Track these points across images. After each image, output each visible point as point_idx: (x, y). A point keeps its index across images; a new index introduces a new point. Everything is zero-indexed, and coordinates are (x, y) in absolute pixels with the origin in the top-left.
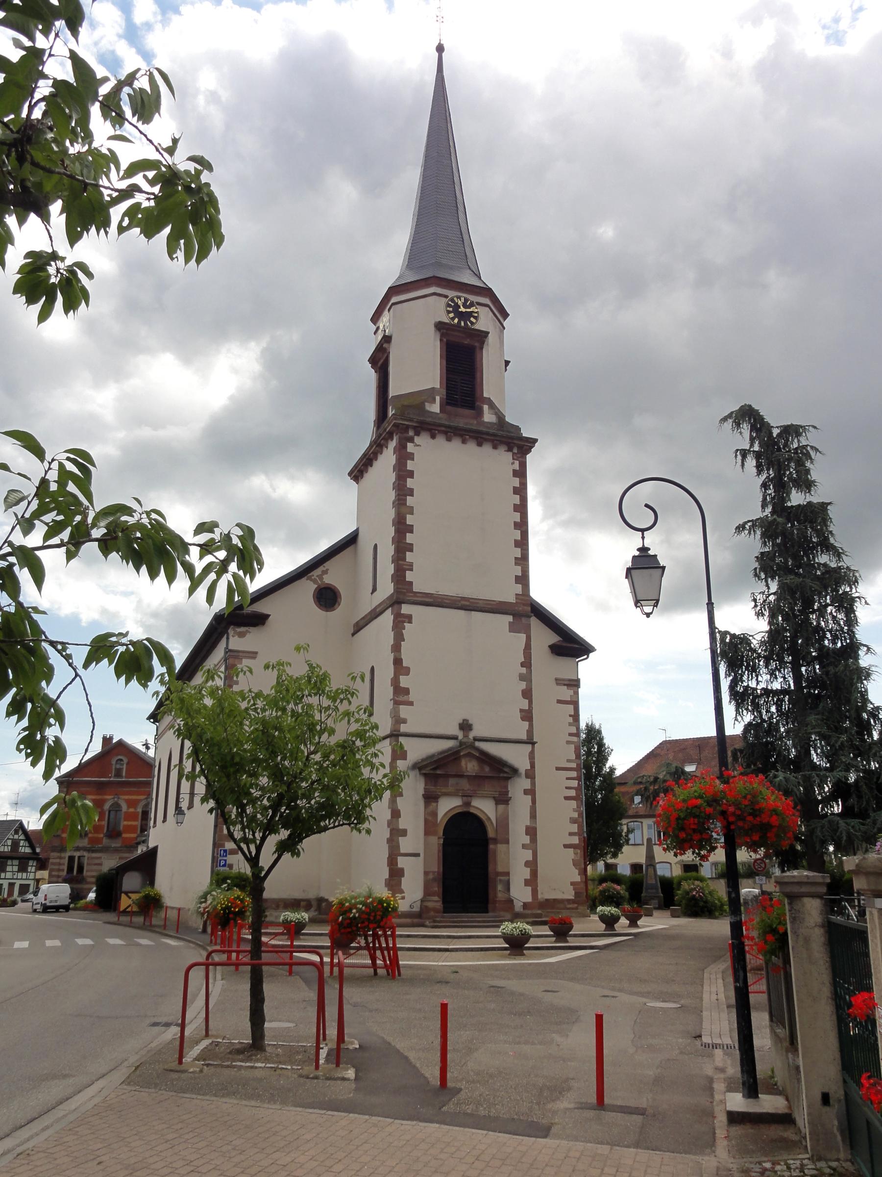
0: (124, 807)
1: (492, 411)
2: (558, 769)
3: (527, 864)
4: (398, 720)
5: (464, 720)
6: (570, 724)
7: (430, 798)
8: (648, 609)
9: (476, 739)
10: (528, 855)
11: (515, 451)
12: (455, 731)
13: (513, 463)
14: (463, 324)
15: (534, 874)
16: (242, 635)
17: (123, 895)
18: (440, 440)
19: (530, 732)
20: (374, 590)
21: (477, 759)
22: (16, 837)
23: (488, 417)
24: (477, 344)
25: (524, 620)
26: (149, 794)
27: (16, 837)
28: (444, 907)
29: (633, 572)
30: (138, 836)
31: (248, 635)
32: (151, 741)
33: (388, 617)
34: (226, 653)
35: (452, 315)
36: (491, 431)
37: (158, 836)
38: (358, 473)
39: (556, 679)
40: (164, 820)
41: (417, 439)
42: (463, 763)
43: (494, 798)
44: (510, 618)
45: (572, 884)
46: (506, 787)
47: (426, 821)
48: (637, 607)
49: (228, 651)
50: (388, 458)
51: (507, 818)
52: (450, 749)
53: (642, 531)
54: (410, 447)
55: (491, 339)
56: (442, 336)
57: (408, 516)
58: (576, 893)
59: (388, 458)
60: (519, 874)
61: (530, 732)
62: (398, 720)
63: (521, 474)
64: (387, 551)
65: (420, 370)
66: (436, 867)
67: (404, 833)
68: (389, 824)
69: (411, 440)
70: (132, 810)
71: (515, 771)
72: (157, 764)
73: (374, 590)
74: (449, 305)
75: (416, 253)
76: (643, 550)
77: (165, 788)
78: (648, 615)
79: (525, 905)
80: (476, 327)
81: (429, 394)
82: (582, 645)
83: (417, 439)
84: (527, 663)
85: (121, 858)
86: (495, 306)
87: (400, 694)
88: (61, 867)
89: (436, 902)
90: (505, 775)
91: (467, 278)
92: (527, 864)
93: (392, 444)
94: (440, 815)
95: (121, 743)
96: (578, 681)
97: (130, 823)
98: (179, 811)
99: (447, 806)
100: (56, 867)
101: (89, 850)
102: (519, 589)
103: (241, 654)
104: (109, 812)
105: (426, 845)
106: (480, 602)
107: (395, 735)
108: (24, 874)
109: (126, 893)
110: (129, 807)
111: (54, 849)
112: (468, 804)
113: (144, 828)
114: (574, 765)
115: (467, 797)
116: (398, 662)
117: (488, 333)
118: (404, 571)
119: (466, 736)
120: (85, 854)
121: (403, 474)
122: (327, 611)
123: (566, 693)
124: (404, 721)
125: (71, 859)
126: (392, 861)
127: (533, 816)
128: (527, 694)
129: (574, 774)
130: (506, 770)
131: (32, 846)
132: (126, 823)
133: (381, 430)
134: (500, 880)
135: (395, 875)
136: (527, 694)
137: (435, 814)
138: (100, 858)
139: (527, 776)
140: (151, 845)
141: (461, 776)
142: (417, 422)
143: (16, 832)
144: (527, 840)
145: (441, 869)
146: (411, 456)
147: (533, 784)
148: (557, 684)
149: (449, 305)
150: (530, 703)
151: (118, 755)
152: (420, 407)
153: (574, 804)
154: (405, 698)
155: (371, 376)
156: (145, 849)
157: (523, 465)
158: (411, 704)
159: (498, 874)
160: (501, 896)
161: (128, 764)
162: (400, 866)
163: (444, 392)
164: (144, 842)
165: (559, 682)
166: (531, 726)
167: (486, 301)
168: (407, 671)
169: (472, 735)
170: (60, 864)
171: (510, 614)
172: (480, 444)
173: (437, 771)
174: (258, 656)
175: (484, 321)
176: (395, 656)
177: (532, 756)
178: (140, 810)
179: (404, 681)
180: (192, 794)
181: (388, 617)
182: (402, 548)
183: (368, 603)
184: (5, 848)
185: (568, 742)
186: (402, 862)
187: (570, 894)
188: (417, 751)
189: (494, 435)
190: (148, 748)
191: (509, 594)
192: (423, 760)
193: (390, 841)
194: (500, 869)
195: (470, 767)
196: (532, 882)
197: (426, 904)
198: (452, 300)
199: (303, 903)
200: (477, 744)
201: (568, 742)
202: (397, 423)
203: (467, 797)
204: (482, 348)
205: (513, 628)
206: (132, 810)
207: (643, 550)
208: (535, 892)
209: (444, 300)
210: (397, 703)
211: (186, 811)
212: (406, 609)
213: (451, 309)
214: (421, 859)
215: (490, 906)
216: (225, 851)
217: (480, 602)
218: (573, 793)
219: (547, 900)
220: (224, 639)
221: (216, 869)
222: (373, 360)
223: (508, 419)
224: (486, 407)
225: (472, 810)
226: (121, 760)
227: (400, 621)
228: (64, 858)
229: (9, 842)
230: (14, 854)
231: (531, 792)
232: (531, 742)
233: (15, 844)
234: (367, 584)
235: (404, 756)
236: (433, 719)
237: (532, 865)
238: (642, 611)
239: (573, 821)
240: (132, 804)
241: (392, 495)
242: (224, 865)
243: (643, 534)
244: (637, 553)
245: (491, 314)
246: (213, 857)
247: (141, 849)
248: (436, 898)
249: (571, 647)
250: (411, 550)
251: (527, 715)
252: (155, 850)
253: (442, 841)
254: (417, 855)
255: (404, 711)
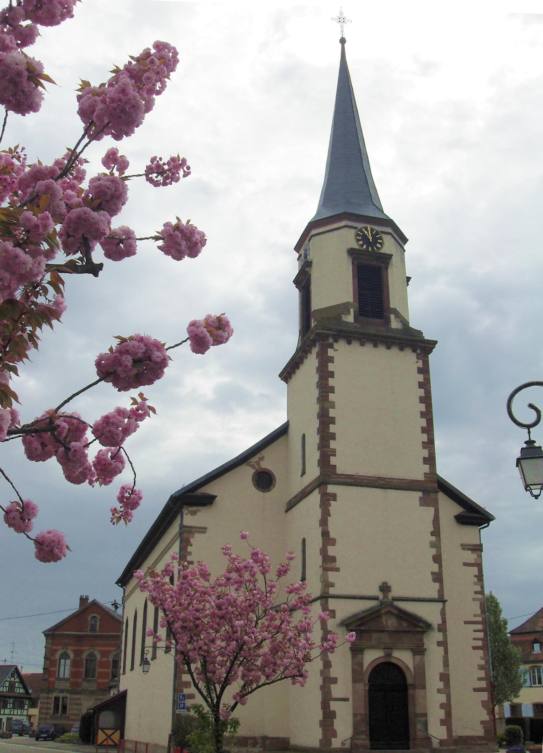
0: (98, 656)
1: (398, 320)
2: (466, 623)
3: (442, 706)
4: (327, 584)
5: (383, 583)
6: (475, 584)
7: (356, 651)
8: (536, 492)
9: (394, 599)
10: (443, 698)
11: (419, 351)
12: (375, 592)
13: (417, 362)
14: (370, 249)
15: (449, 714)
16: (193, 513)
17: (100, 731)
18: (356, 346)
19: (441, 591)
20: (304, 473)
21: (397, 616)
22: (12, 679)
23: (395, 324)
24: (383, 265)
25: (432, 495)
26: (119, 647)
27: (12, 679)
28: (371, 745)
29: (522, 461)
30: (110, 681)
31: (199, 513)
32: (119, 601)
33: (315, 497)
34: (181, 528)
35: (361, 243)
36: (398, 336)
37: (130, 681)
38: (287, 374)
39: (462, 545)
40: (132, 669)
41: (336, 346)
42: (384, 619)
43: (411, 649)
44: (420, 494)
45: (482, 722)
46: (422, 640)
47: (354, 671)
48: (527, 490)
49: (182, 526)
50: (311, 362)
51: (423, 667)
52: (372, 608)
53: (529, 427)
54: (330, 352)
55: (395, 260)
56: (353, 260)
57: (331, 410)
58: (485, 731)
59: (311, 362)
60: (435, 715)
61: (441, 591)
62: (327, 584)
63: (424, 370)
64: (313, 440)
65: (336, 288)
66: (363, 710)
67: (334, 681)
68: (322, 673)
69: (331, 346)
70: (105, 659)
71: (428, 626)
72: (125, 621)
73: (304, 473)
74: (358, 235)
75: (329, 195)
76: (530, 442)
77: (131, 643)
78: (536, 497)
79: (442, 742)
80: (382, 251)
81: (344, 308)
82: (482, 514)
83: (336, 346)
84: (436, 532)
85: (96, 700)
86: (397, 235)
87: (329, 562)
88: (49, 706)
89: (364, 740)
90: (420, 629)
91: (372, 213)
92: (442, 706)
93: (315, 350)
94: (365, 666)
95: (95, 604)
96: (481, 545)
97: (103, 670)
98: (144, 662)
99: (371, 657)
100: (45, 706)
101: (71, 692)
102: (426, 468)
103: (193, 529)
104: (87, 660)
105: (354, 692)
106: (394, 481)
107: (324, 597)
108: (19, 711)
109: (102, 730)
110: (102, 657)
111: (42, 690)
112: (389, 655)
113: (115, 675)
114: (480, 619)
115: (388, 649)
116: (325, 534)
117: (392, 255)
118: (329, 456)
119: (385, 596)
120: (68, 695)
121: (324, 374)
122: (264, 492)
123: (471, 557)
124: (332, 585)
125: (57, 699)
126: (325, 705)
127: (446, 664)
128: (437, 559)
129: (480, 627)
130: (421, 624)
131: (25, 687)
132: (100, 670)
133: (305, 338)
134: (419, 720)
135: (328, 717)
136: (437, 559)
137: (361, 665)
138: (79, 699)
139: (439, 630)
140: (122, 689)
141: (382, 631)
142: (336, 331)
143: (13, 676)
144: (441, 685)
145: (368, 712)
146: (331, 360)
147: (445, 636)
148: (463, 549)
149: (358, 235)
150: (440, 567)
151: (94, 613)
152: (338, 319)
153: (480, 653)
154: (333, 565)
155: (295, 293)
156: (116, 692)
157: (426, 363)
158: (338, 570)
159: (416, 715)
160: (420, 734)
161: (100, 620)
162: (332, 708)
163: (357, 305)
164: (115, 686)
165: (464, 547)
166: (441, 586)
167: (389, 230)
168: (333, 542)
169: (391, 595)
170: (48, 703)
171: (420, 491)
172: (389, 348)
173: (363, 626)
174: (208, 531)
175: (388, 246)
176: (323, 529)
177: (443, 613)
178: (111, 659)
179: (331, 551)
180: (155, 647)
181: (315, 497)
182: (326, 436)
183: (299, 484)
184: (4, 689)
185: (474, 599)
186: (334, 706)
187: (479, 731)
188: (345, 609)
189: (399, 339)
190: (117, 607)
191: (418, 472)
192: (349, 618)
193: (322, 688)
194: (419, 711)
195: (391, 623)
196: (447, 722)
197: (355, 741)
198: (361, 231)
199: (250, 741)
200: (396, 603)
201: (474, 599)
202: (318, 332)
203: (388, 649)
204: (387, 268)
205: (424, 502)
206: (105, 659)
207: (530, 442)
208: (449, 731)
209: (353, 231)
210: (325, 569)
211: (150, 662)
212: (331, 489)
213: (360, 238)
214: (350, 703)
215: (411, 744)
216: (184, 696)
217: (394, 481)
218: (480, 643)
219: (460, 737)
220: (179, 517)
221: (177, 712)
222: (297, 282)
223: (411, 325)
224: (392, 317)
225: (393, 661)
226: (95, 617)
227: (327, 500)
228: (51, 698)
229: (7, 684)
230: (11, 694)
231: (443, 644)
232: (441, 600)
233: (12, 686)
234: (296, 470)
235: (333, 614)
236: (358, 580)
237: (447, 707)
238: (531, 493)
239: (481, 667)
240: (105, 654)
241: (315, 393)
242: (183, 708)
243: (529, 430)
244: (525, 446)
245: (393, 240)
246: (174, 701)
247: (113, 693)
248: (364, 737)
249: (474, 516)
250: (334, 439)
251: (438, 577)
252: (125, 692)
253: (367, 688)
254: (346, 700)
255: (332, 576)
